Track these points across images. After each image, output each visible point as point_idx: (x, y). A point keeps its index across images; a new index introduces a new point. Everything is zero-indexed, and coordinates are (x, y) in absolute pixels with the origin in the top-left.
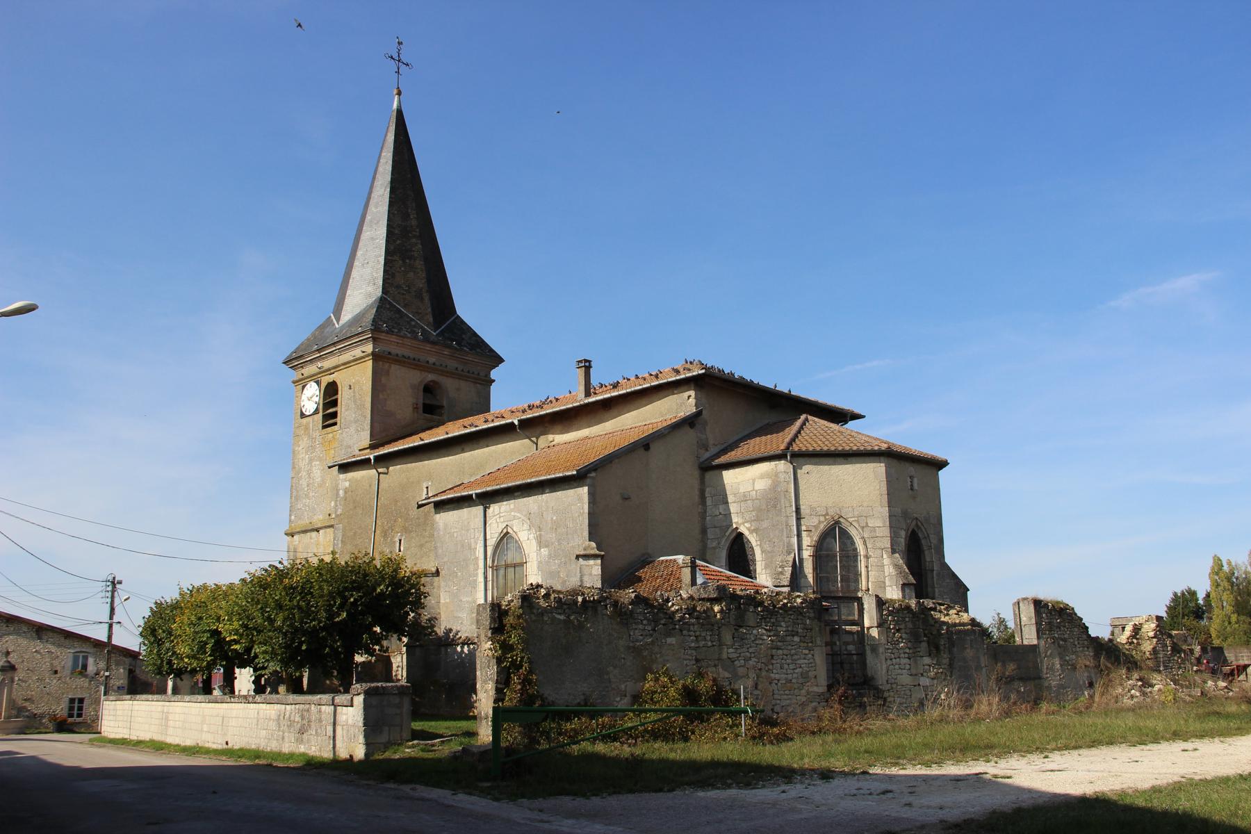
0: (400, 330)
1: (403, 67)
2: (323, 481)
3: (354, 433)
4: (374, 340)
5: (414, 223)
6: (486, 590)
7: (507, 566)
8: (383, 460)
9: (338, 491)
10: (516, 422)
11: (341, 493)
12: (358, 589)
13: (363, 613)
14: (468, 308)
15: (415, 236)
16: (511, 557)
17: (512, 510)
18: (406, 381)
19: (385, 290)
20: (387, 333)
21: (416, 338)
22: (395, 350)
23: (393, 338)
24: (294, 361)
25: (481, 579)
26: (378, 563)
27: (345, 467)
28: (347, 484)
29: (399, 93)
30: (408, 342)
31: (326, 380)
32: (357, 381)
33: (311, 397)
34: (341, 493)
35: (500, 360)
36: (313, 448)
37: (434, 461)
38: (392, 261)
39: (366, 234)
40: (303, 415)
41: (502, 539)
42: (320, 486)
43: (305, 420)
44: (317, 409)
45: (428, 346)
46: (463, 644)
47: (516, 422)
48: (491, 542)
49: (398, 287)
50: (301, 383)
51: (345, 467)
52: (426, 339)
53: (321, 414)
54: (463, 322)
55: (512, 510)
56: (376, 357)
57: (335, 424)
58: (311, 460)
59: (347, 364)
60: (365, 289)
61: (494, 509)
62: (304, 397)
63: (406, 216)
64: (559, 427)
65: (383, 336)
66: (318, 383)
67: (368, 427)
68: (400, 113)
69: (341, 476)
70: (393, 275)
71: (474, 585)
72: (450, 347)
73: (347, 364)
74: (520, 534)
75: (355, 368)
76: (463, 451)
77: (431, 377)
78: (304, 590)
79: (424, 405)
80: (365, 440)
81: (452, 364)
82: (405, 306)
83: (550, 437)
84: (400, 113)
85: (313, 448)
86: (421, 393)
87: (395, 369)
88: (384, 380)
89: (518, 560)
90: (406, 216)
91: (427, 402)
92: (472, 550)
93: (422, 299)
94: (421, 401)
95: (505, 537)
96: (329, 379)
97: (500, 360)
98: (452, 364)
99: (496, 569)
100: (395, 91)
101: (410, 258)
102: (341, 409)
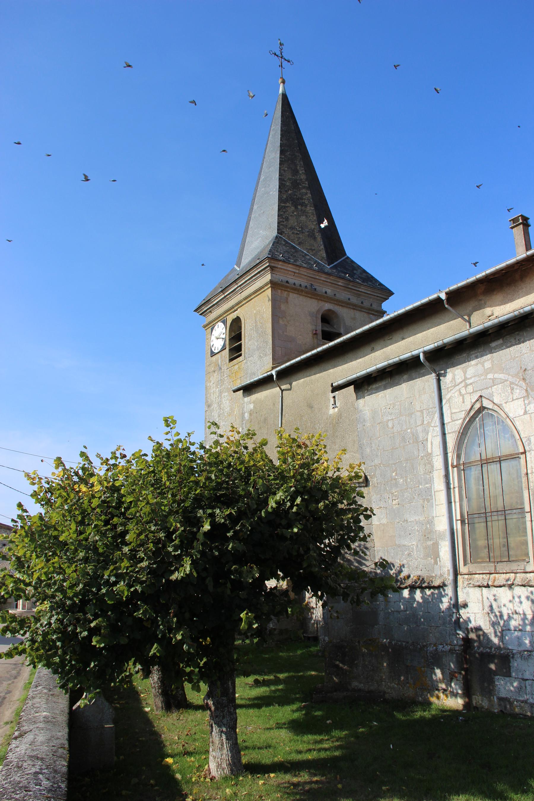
0: (296, 261)
1: (285, 63)
2: (232, 410)
3: (259, 360)
4: (272, 269)
5: (303, 177)
6: (449, 503)
7: (485, 462)
8: (286, 375)
9: (243, 414)
10: (443, 296)
11: (247, 415)
12: (227, 501)
13: (240, 558)
14: (354, 249)
15: (304, 187)
16: (491, 443)
17: (487, 372)
18: (305, 311)
19: (280, 231)
20: (284, 261)
21: (311, 268)
22: (292, 280)
23: (290, 268)
24: (203, 308)
25: (439, 485)
26: (273, 453)
27: (249, 389)
28: (252, 406)
29: (283, 82)
30: (303, 271)
31: (230, 318)
32: (257, 313)
33: (220, 331)
34: (247, 415)
35: (391, 293)
36: (222, 381)
37: (340, 368)
38: (285, 207)
39: (261, 190)
40: (213, 354)
41: (472, 419)
42: (229, 415)
43: (214, 358)
44: (224, 345)
45: (323, 277)
46: (412, 588)
47: (443, 296)
48: (453, 427)
49: (292, 228)
50: (210, 326)
51: (249, 389)
52: (321, 271)
53: (227, 349)
54: (352, 262)
55: (487, 372)
56: (274, 284)
57: (240, 355)
58: (221, 393)
59: (248, 298)
60: (262, 231)
61: (454, 375)
62: (213, 338)
63: (295, 172)
64: (498, 297)
65: (280, 265)
66: (225, 322)
67: (269, 351)
68: (285, 97)
69: (247, 399)
70: (287, 219)
71: (427, 496)
72: (344, 278)
73: (248, 298)
74: (507, 408)
75: (256, 300)
76: (373, 350)
77: (327, 306)
78: (114, 506)
79: (323, 332)
80: (268, 360)
81: (343, 295)
82: (300, 244)
83: (488, 311)
84: (285, 97)
85: (222, 381)
86: (319, 321)
87: (294, 298)
88: (283, 307)
89: (506, 449)
90: (295, 172)
91: (326, 329)
92: (420, 442)
93: (315, 239)
94: (319, 329)
95: (478, 414)
96: (233, 316)
97: (391, 293)
98: (343, 295)
99: (463, 468)
100: (280, 80)
101: (302, 205)
102: (246, 342)
